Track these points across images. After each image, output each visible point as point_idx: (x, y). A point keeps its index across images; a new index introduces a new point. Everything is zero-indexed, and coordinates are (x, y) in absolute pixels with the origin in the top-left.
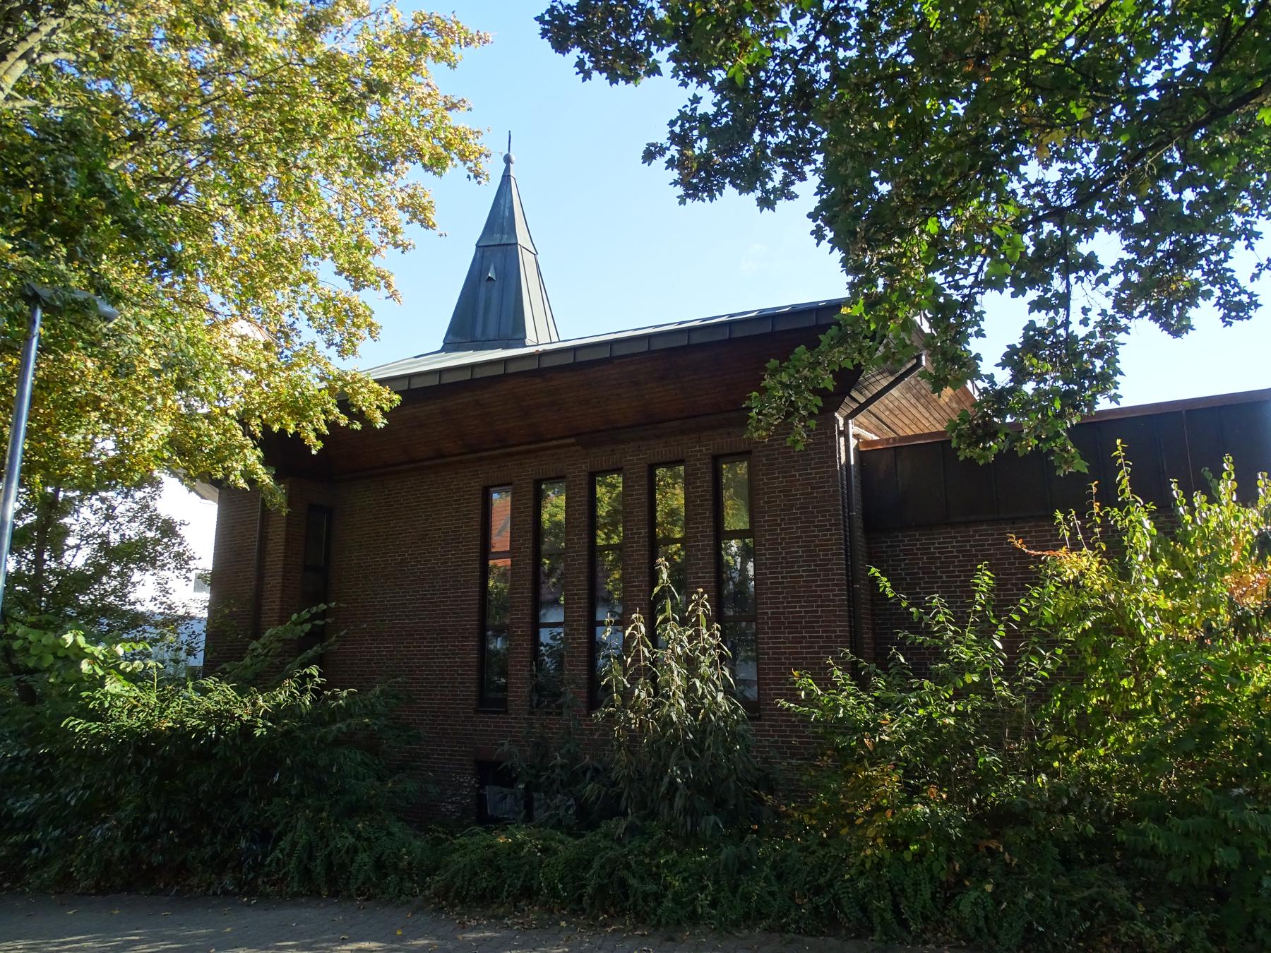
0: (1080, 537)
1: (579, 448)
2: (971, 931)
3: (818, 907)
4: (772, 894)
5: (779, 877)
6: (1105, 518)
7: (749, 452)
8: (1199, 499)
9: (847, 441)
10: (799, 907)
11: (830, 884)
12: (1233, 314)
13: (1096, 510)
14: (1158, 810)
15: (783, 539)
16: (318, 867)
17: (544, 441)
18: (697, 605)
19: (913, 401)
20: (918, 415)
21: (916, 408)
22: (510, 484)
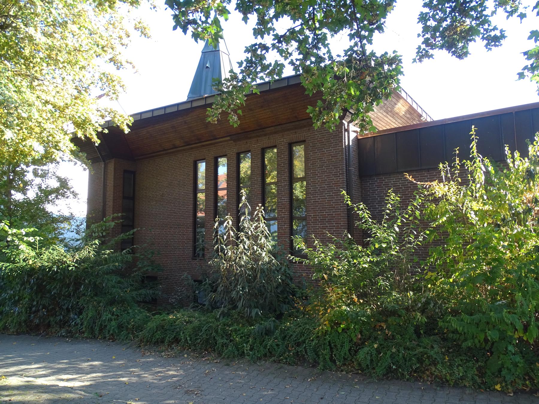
0: (449, 175)
1: (232, 142)
2: (364, 366)
3: (298, 352)
4: (277, 345)
5: (284, 338)
6: (462, 166)
7: (304, 141)
8: (517, 155)
9: (349, 134)
10: (289, 351)
11: (304, 342)
12: (493, 43)
13: (458, 162)
14: (472, 309)
15: (318, 181)
16: (97, 329)
17: (216, 139)
18: (259, 212)
19: (384, 114)
20: (389, 121)
21: (387, 117)
22: (204, 159)
